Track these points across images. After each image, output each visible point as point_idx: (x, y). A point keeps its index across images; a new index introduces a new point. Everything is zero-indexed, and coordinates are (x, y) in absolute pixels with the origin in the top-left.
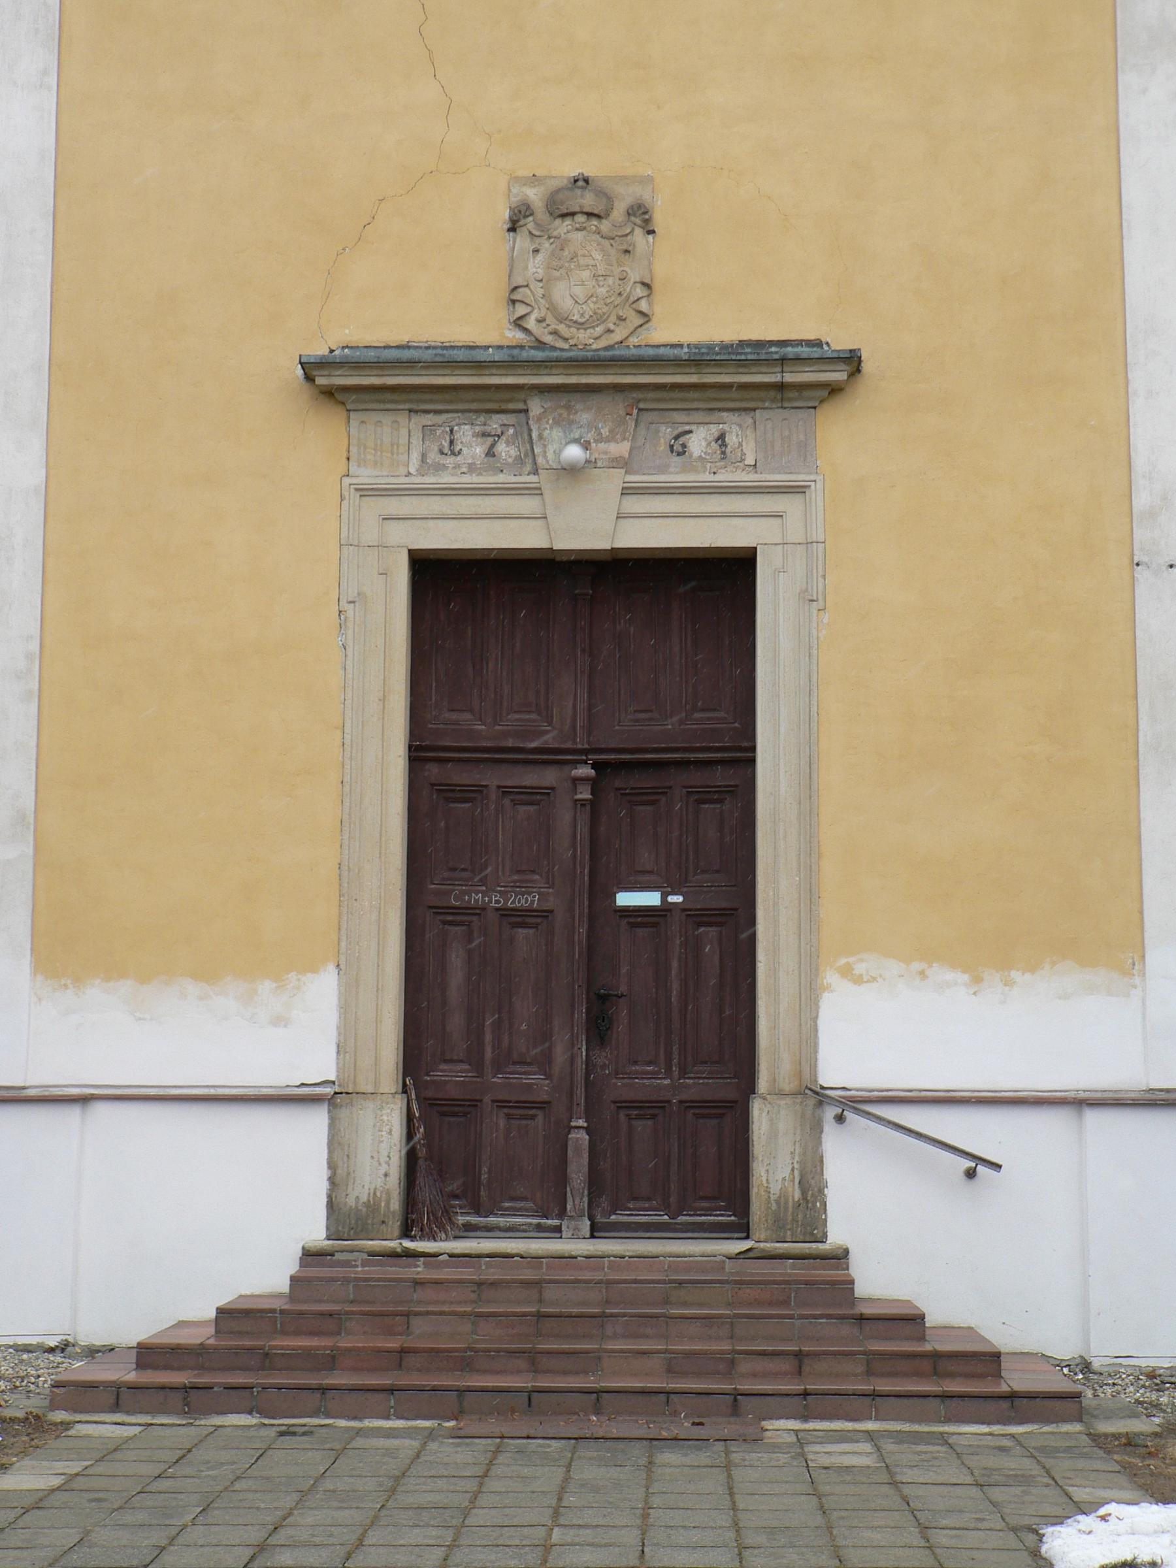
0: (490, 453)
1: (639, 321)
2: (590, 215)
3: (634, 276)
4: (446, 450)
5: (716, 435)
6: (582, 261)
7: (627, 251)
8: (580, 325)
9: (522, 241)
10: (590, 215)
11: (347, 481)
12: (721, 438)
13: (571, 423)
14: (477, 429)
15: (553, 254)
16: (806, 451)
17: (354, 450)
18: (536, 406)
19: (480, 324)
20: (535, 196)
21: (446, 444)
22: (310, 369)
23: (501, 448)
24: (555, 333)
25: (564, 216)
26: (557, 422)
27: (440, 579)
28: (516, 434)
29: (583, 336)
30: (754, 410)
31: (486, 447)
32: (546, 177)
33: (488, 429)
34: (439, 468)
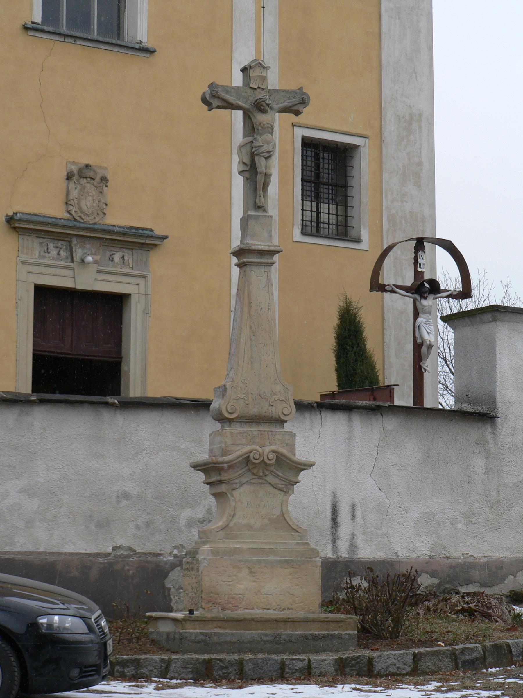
0: (58, 254)
1: (102, 215)
2: (91, 178)
3: (103, 201)
4: (46, 251)
5: (122, 256)
6: (90, 194)
7: (101, 192)
8: (87, 215)
9: (72, 185)
10: (91, 178)
11: (19, 258)
12: (123, 257)
13: (84, 247)
14: (55, 245)
15: (81, 190)
16: (146, 264)
17: (20, 248)
18: (74, 241)
19: (55, 210)
20: (74, 168)
21: (46, 249)
22: (10, 220)
23: (62, 252)
24: (80, 217)
25: (84, 178)
26: (80, 247)
27: (41, 292)
28: (66, 249)
29: (87, 219)
30: (133, 249)
31: (57, 252)
32: (78, 163)
33: (57, 245)
34: (44, 257)
